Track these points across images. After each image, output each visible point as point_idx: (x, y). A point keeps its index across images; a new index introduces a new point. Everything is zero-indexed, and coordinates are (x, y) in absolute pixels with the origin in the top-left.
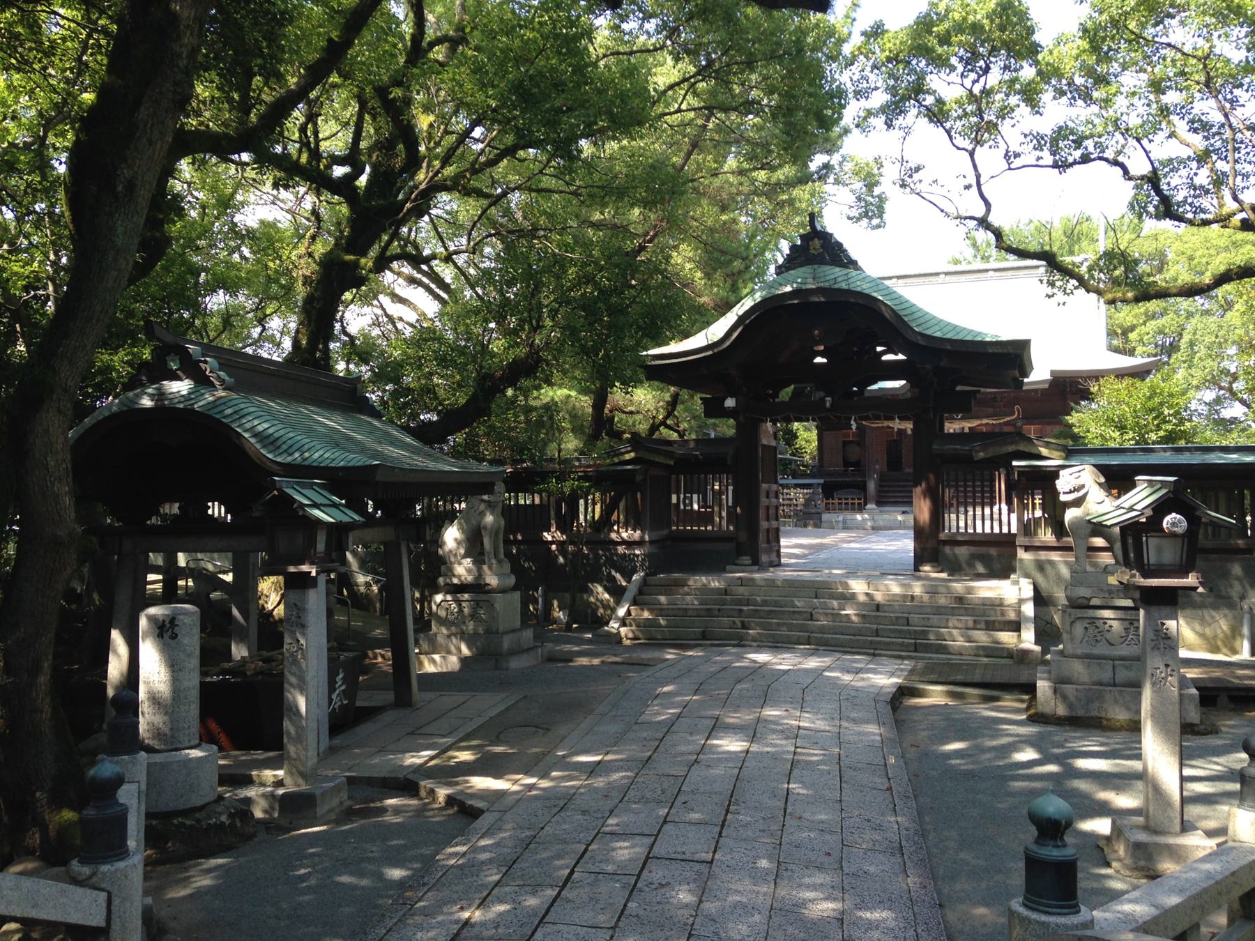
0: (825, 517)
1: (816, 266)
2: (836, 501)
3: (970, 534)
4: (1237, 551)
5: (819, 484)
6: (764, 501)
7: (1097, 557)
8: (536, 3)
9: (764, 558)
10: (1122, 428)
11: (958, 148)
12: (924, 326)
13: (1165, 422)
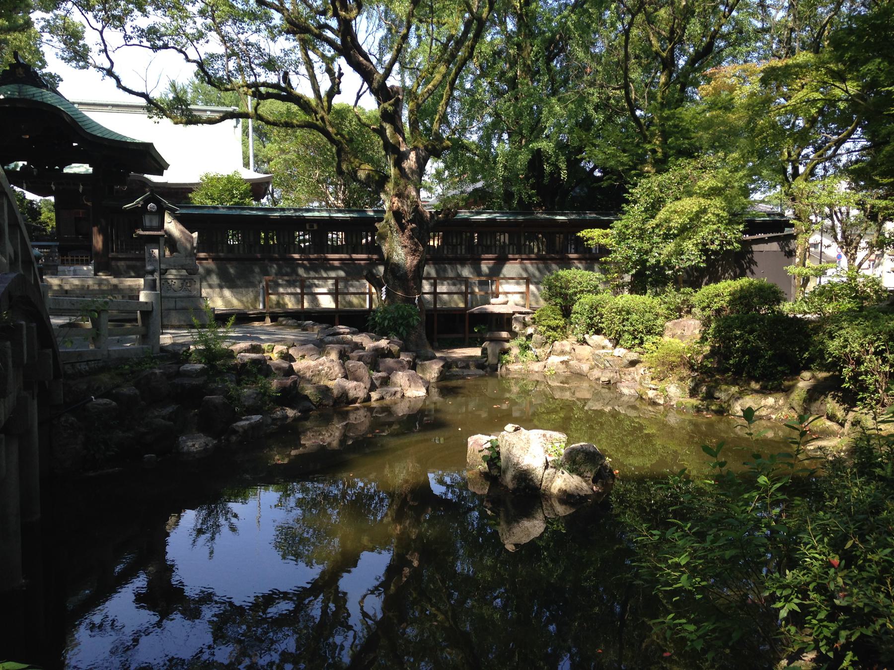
0: (60, 268)
1: (21, 85)
2: (70, 258)
4: (257, 259)
10: (213, 199)
11: (94, 29)
12: (92, 129)
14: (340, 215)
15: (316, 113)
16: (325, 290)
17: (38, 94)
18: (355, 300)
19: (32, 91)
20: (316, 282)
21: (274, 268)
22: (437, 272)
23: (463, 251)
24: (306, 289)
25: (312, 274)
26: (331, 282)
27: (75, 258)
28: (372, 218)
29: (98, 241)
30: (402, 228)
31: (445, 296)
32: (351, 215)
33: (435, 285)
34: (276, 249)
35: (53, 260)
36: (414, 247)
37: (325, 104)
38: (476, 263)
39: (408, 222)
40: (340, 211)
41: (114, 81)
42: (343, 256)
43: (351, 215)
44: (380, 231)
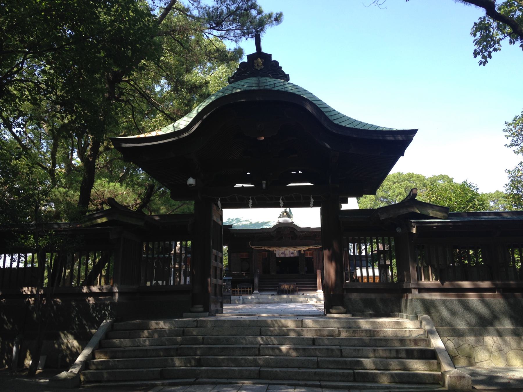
0: (233, 297)
2: (238, 289)
3: (365, 283)
5: (229, 280)
7: (467, 296)
8: (75, 1)
9: (213, 307)
12: (340, 120)
17: (279, 84)
19: (270, 82)
27: (242, 289)
35: (228, 291)
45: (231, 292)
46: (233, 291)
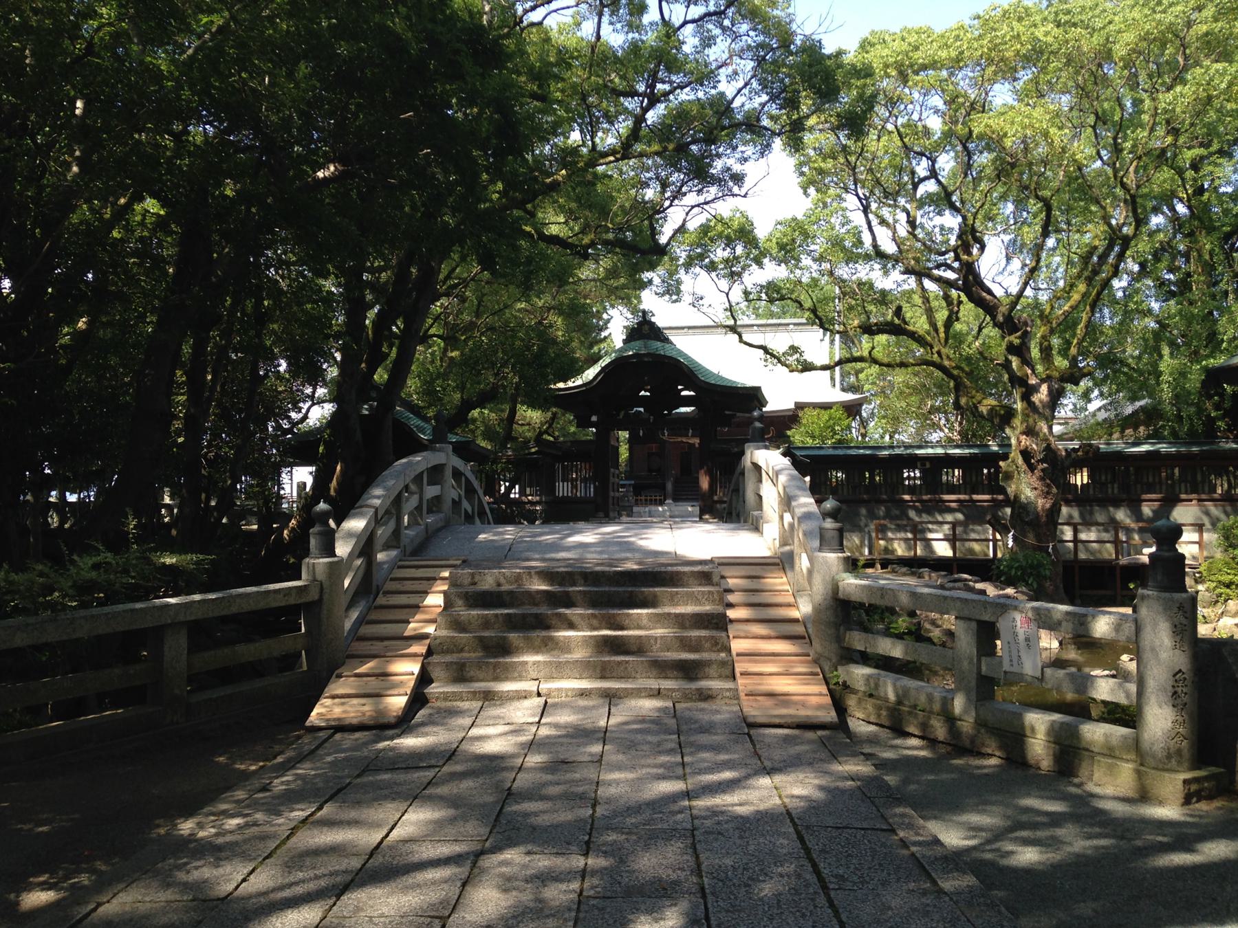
0: (635, 509)
6: (612, 479)
9: (611, 514)
10: (813, 437)
13: (835, 434)
14: (957, 451)
15: (932, 347)
16: (940, 536)
18: (977, 547)
19: (656, 345)
20: (930, 526)
21: (882, 511)
22: (1082, 515)
23: (1116, 491)
24: (919, 532)
25: (925, 517)
26: (946, 527)
28: (995, 454)
29: (705, 483)
30: (1032, 468)
31: (1094, 545)
32: (972, 451)
33: (1076, 532)
34: (883, 490)
36: (1046, 489)
37: (942, 335)
38: (1134, 506)
39: (1038, 461)
40: (957, 447)
41: (736, 337)
42: (962, 497)
43: (972, 451)
44: (1004, 469)
45: (633, 501)
46: (636, 500)
